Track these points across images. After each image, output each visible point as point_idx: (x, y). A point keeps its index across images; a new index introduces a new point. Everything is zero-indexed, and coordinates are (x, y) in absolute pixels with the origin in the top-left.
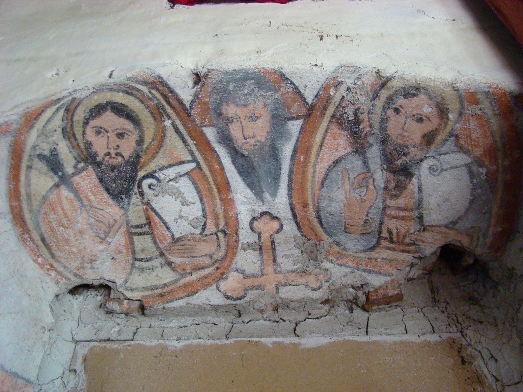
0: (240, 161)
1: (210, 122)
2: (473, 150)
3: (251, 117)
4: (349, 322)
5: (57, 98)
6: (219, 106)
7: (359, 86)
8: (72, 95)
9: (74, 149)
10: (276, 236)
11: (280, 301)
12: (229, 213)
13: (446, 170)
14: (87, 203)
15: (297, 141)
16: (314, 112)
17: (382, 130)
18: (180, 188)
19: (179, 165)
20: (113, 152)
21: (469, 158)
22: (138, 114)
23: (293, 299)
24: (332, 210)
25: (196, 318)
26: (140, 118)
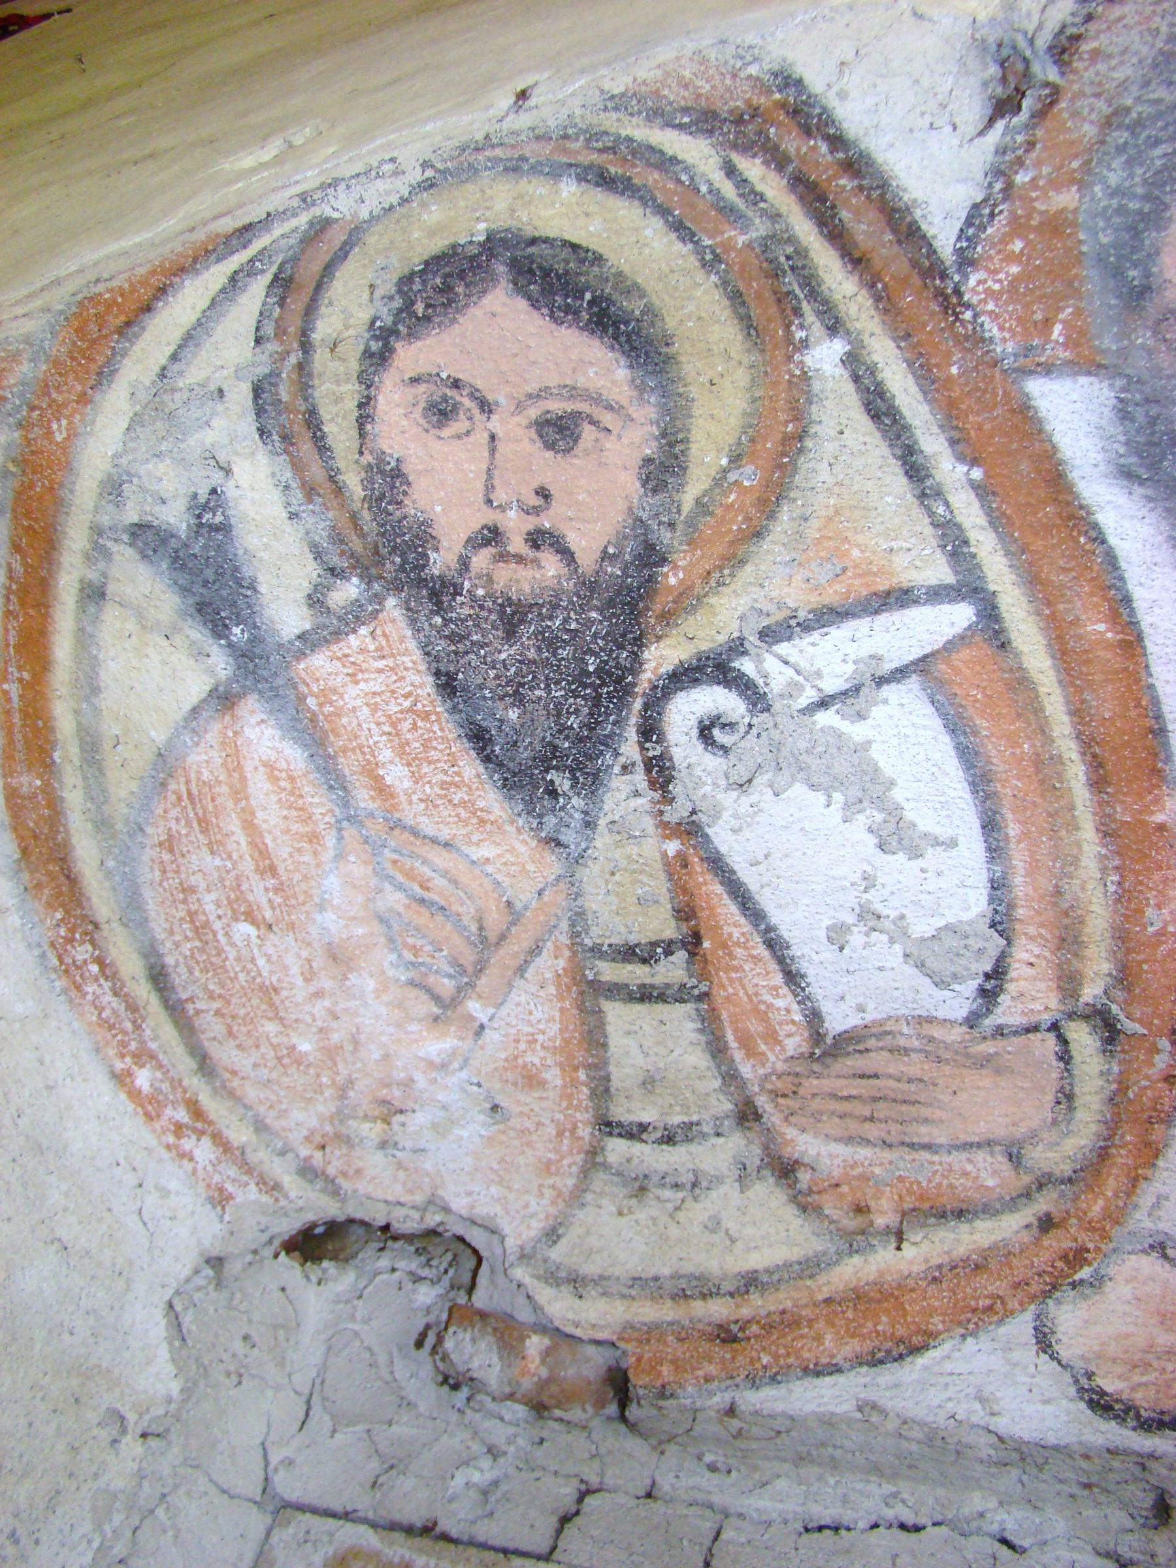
1: (1077, 345)
5: (239, 224)
8: (314, 204)
9: (310, 501)
12: (1150, 913)
14: (372, 806)
18: (875, 753)
19: (877, 612)
20: (515, 524)
22: (656, 301)
25: (905, 1488)
26: (671, 323)
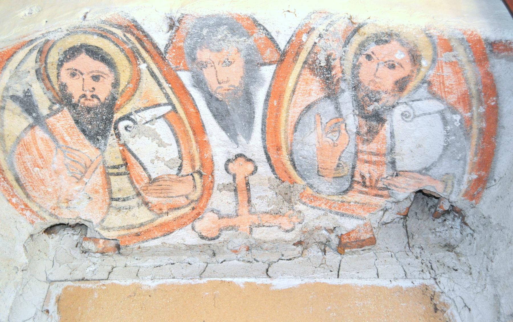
0: (215, 104)
1: (185, 67)
2: (446, 97)
3: (225, 62)
4: (321, 265)
6: (193, 51)
7: (331, 32)
8: (45, 36)
9: (48, 91)
10: (251, 178)
11: (253, 242)
13: (418, 116)
14: (63, 144)
15: (270, 86)
16: (286, 57)
17: (353, 77)
18: (156, 130)
20: (89, 94)
21: (443, 105)
22: (113, 57)
23: (266, 240)
24: (305, 153)
25: (172, 257)
26: (116, 61)
